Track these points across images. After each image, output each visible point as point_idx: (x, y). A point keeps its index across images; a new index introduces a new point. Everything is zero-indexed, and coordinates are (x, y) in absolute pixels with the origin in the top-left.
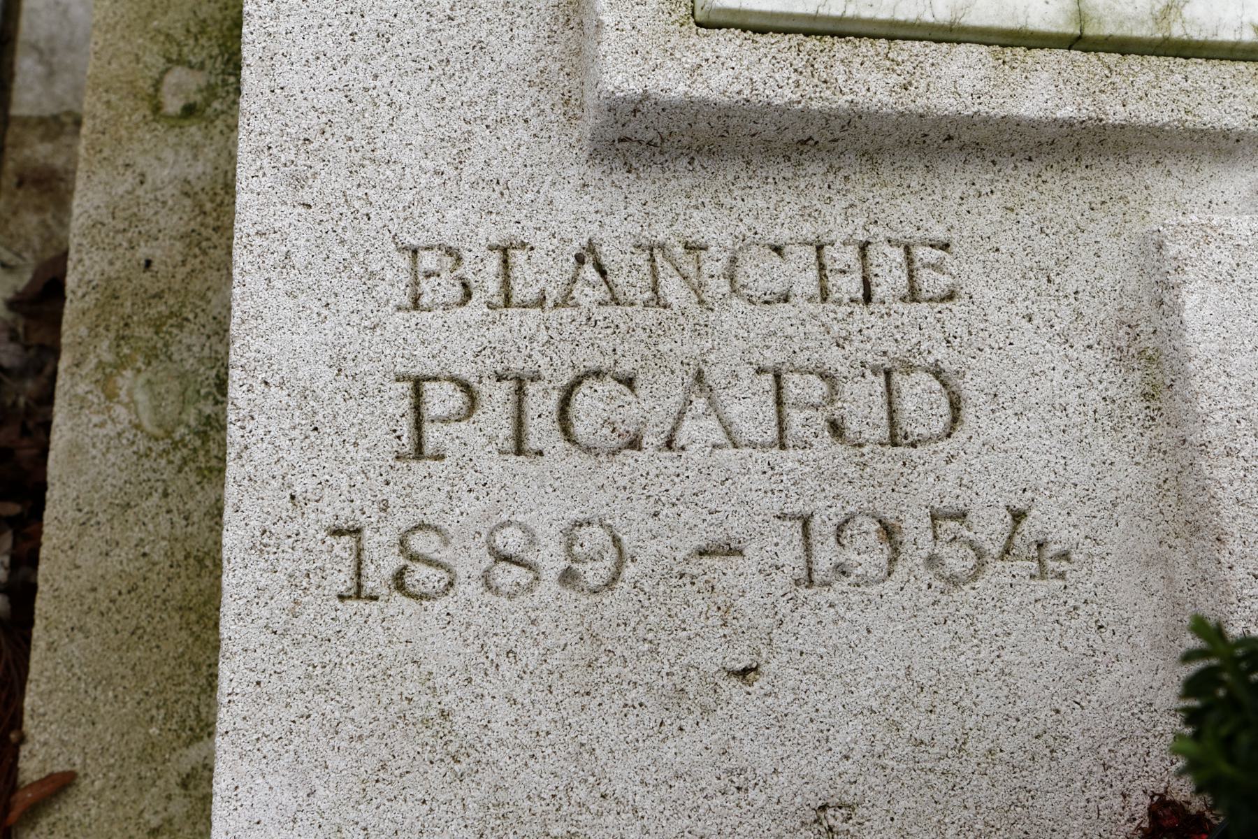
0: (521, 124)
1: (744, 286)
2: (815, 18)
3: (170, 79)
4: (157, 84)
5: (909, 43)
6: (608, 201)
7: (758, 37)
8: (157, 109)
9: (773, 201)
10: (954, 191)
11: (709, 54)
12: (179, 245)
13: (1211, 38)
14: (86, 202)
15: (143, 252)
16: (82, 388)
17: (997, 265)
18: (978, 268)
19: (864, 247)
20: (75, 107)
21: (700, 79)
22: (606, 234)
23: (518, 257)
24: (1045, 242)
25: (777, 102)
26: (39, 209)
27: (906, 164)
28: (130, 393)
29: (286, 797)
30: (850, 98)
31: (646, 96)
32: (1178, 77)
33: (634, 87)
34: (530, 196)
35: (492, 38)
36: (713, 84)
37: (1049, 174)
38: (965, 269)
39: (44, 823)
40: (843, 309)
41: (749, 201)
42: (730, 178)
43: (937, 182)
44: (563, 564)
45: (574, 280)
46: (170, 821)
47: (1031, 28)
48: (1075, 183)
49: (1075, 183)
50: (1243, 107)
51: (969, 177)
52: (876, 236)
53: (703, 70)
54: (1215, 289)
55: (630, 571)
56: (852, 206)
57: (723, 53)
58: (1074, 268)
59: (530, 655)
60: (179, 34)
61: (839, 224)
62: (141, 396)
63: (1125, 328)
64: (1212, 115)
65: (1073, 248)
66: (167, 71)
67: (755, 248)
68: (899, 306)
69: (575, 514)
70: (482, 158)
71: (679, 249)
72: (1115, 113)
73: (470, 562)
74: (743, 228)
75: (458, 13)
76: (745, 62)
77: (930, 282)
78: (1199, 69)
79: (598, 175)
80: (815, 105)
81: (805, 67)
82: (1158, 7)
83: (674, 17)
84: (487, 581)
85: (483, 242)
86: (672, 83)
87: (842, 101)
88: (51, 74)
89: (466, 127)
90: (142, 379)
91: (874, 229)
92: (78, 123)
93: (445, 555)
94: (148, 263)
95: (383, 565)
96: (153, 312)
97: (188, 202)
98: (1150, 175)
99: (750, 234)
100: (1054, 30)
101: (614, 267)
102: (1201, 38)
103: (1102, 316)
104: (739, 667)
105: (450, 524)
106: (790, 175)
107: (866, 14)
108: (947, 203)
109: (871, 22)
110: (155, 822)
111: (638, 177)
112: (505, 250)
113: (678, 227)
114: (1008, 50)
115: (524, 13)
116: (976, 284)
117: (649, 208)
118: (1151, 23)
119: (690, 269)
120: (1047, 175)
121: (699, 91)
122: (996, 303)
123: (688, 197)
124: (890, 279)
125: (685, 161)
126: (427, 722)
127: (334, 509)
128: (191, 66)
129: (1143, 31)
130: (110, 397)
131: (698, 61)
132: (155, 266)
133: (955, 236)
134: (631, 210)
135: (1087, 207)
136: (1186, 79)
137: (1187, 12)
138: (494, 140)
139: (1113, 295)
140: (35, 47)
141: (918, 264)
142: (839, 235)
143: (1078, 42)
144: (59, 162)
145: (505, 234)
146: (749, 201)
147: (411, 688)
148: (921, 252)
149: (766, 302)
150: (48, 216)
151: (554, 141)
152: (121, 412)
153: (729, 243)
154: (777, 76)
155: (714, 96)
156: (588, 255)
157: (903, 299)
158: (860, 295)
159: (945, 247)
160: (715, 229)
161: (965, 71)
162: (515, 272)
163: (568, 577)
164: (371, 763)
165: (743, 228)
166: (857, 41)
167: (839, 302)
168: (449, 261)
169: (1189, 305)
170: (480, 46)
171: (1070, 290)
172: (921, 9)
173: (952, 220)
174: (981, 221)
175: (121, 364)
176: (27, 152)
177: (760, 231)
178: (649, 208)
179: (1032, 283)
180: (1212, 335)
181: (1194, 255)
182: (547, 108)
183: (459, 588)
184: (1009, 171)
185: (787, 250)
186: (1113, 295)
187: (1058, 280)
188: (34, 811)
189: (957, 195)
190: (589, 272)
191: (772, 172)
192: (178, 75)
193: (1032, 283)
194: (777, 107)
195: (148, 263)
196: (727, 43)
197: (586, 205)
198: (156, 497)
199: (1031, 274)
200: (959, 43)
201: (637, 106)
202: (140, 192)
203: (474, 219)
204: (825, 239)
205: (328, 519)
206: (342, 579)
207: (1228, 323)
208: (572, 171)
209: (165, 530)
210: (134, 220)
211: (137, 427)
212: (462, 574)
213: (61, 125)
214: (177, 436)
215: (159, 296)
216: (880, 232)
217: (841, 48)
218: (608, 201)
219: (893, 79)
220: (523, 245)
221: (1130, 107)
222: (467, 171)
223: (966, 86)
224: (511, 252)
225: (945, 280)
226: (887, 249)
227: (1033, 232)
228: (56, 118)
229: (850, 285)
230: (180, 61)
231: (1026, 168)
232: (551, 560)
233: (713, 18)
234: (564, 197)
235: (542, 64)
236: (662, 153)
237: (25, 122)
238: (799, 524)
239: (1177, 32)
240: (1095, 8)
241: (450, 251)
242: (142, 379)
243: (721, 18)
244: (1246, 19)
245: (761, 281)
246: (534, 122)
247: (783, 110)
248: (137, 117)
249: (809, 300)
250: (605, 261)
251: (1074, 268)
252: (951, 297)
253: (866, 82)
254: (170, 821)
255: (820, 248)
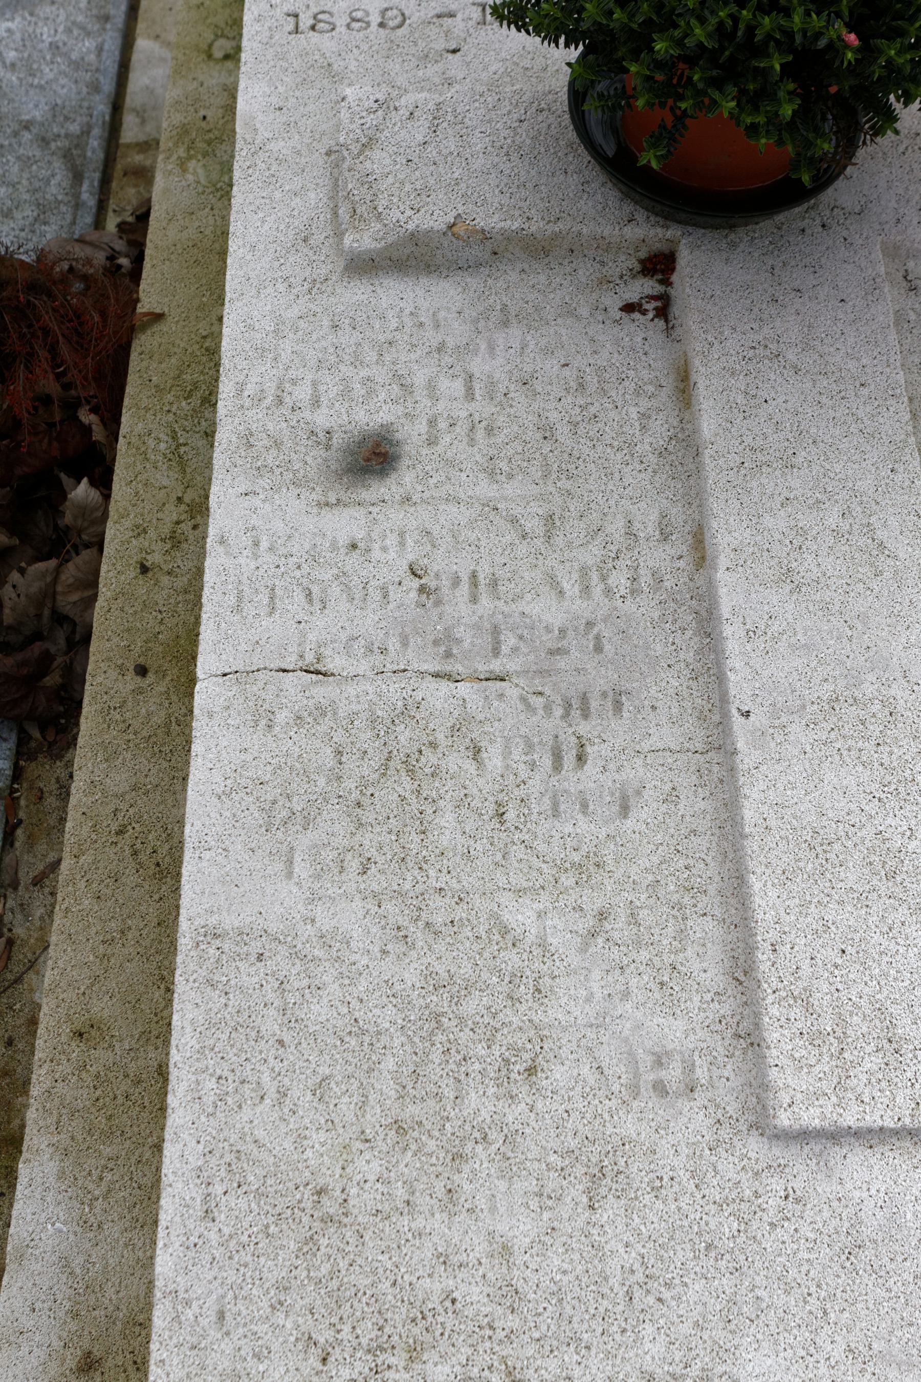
3: (218, 44)
4: (210, 46)
8: (210, 56)
12: (221, 110)
14: (160, 182)
15: (202, 113)
16: (170, 167)
20: (157, 136)
26: (135, 186)
28: (194, 169)
29: (266, 89)
39: (149, 332)
44: (379, 20)
46: (212, 334)
55: (408, 22)
59: (365, 47)
60: (222, 25)
62: (200, 171)
66: (215, 40)
69: (386, 5)
73: (341, 21)
84: (348, 26)
88: (143, 122)
90: (201, 164)
92: (158, 143)
93: (331, 20)
94: (204, 118)
95: (306, 21)
96: (207, 137)
97: (226, 94)
104: (451, 48)
105: (335, 10)
110: (204, 333)
126: (322, 67)
127: (288, 7)
128: (228, 38)
130: (184, 171)
132: (208, 119)
140: (134, 110)
144: (148, 163)
147: (317, 57)
150: (141, 189)
152: (190, 177)
163: (382, 25)
164: (299, 80)
175: (190, 158)
176: (129, 160)
183: (337, 30)
188: (144, 327)
192: (221, 42)
195: (204, 118)
198: (207, 210)
202: (201, 89)
205: (285, 10)
206: (291, 27)
209: (211, 222)
210: (198, 100)
211: (198, 182)
212: (338, 24)
213: (149, 146)
214: (218, 186)
215: (210, 131)
228: (146, 143)
230: (222, 36)
232: (375, 19)
237: (128, 146)
238: (480, 9)
242: (201, 164)
248: (199, 59)
254: (212, 334)
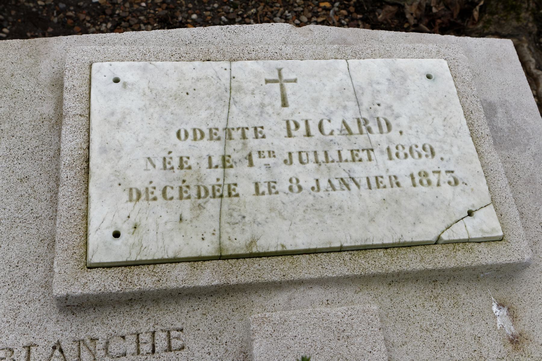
0: (38, 302)
1: (110, 352)
2: (127, 262)
5: (161, 265)
6: (65, 326)
7: (108, 270)
9: (122, 320)
10: (185, 310)
11: (90, 278)
13: (266, 251)
17: (198, 335)
18: (192, 337)
19: (154, 333)
21: (87, 287)
22: (63, 338)
23: (33, 349)
24: (216, 325)
25: (113, 291)
27: (169, 302)
30: (138, 287)
31: (68, 295)
32: (256, 265)
33: (64, 293)
34: (39, 327)
35: (30, 272)
36: (91, 288)
37: (219, 300)
38: (188, 338)
40: (143, 357)
41: (114, 321)
42: (108, 313)
43: (179, 307)
45: (52, 355)
47: (202, 255)
48: (227, 303)
49: (227, 303)
50: (279, 273)
51: (190, 304)
52: (157, 329)
53: (88, 284)
54: (265, 341)
56: (149, 319)
57: (95, 277)
58: (226, 333)
61: (144, 326)
63: (243, 354)
64: (268, 277)
65: (226, 326)
67: (115, 337)
68: (163, 354)
70: (23, 315)
71: (88, 341)
72: (233, 280)
74: (111, 331)
75: (20, 264)
76: (103, 279)
77: (176, 344)
78: (264, 261)
79: (62, 317)
80: (127, 291)
81: (124, 278)
82: (248, 242)
83: (79, 266)
85: (21, 345)
86: (77, 290)
87: (136, 288)
89: (19, 305)
91: (156, 327)
98: (254, 297)
99: (113, 333)
100: (211, 255)
101: (65, 350)
102: (263, 251)
103: (235, 350)
106: (128, 310)
107: (144, 258)
108: (182, 314)
109: (146, 260)
111: (76, 316)
112: (29, 347)
113: (88, 333)
114: (196, 264)
115: (42, 262)
116: (191, 344)
117: (79, 327)
118: (245, 249)
119: (92, 348)
120: (217, 301)
121: (86, 291)
122: (197, 349)
123: (93, 322)
124: (161, 342)
125: (92, 309)
129: (242, 252)
131: (86, 281)
133: (184, 326)
134: (73, 328)
135: (231, 311)
136: (259, 265)
137: (258, 243)
138: (28, 308)
139: (239, 342)
141: (171, 338)
142: (144, 330)
143: (220, 258)
145: (29, 342)
146: (114, 321)
148: (174, 334)
149: (118, 357)
151: (48, 306)
153: (105, 337)
154: (113, 283)
155: (91, 292)
156: (57, 347)
157: (166, 351)
158: (150, 351)
159: (182, 330)
160: (100, 333)
161: (180, 273)
162: (32, 355)
165: (111, 331)
166: (143, 267)
167: (143, 355)
168: (9, 353)
169: (255, 347)
170: (26, 275)
171: (224, 342)
172: (163, 254)
173: (183, 321)
174: (194, 320)
177: (117, 331)
178: (79, 327)
179: (210, 341)
180: (263, 358)
181: (258, 329)
182: (47, 295)
184: (204, 301)
185: (126, 337)
186: (239, 342)
187: (220, 339)
189: (186, 311)
190: (57, 353)
191: (123, 310)
193: (210, 341)
194: (114, 293)
196: (96, 274)
197: (58, 329)
199: (211, 337)
200: (179, 262)
201: (67, 297)
203: (18, 337)
204: (139, 332)
207: (269, 353)
208: (54, 316)
216: (158, 327)
217: (136, 270)
218: (65, 326)
219: (155, 278)
220: (35, 345)
221: (238, 278)
222: (18, 320)
223: (180, 277)
224: (31, 347)
225: (180, 343)
226: (161, 333)
227: (212, 322)
229: (146, 348)
231: (210, 299)
233: (92, 266)
234: (51, 326)
235: (47, 279)
236: (83, 307)
239: (254, 250)
240: (226, 246)
241: (10, 350)
243: (95, 265)
244: (279, 243)
245: (116, 350)
246: (43, 301)
247: (117, 293)
249: (133, 355)
250: (63, 348)
251: (226, 333)
252: (183, 348)
253: (145, 281)
255: (138, 335)
